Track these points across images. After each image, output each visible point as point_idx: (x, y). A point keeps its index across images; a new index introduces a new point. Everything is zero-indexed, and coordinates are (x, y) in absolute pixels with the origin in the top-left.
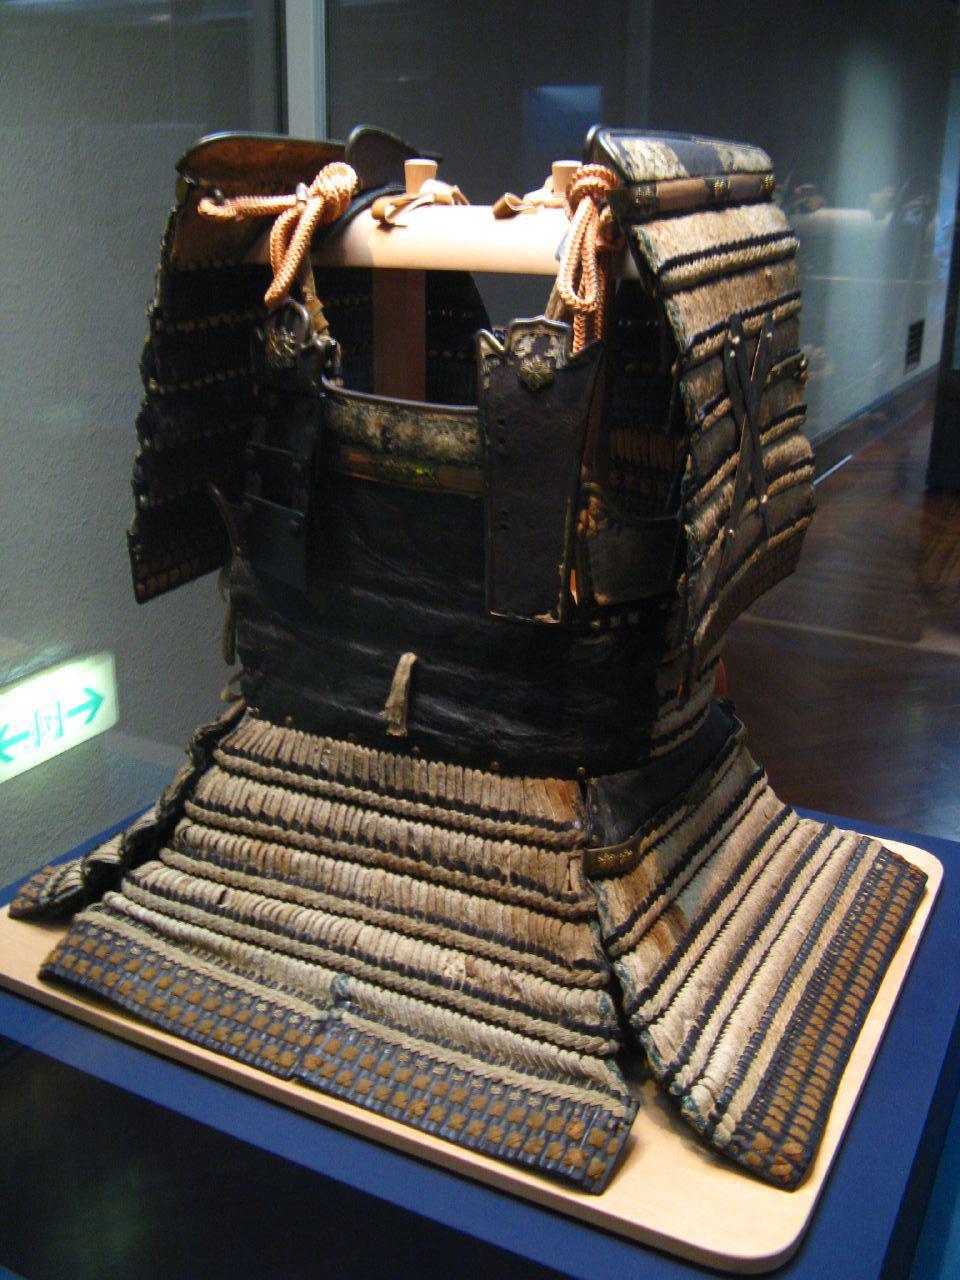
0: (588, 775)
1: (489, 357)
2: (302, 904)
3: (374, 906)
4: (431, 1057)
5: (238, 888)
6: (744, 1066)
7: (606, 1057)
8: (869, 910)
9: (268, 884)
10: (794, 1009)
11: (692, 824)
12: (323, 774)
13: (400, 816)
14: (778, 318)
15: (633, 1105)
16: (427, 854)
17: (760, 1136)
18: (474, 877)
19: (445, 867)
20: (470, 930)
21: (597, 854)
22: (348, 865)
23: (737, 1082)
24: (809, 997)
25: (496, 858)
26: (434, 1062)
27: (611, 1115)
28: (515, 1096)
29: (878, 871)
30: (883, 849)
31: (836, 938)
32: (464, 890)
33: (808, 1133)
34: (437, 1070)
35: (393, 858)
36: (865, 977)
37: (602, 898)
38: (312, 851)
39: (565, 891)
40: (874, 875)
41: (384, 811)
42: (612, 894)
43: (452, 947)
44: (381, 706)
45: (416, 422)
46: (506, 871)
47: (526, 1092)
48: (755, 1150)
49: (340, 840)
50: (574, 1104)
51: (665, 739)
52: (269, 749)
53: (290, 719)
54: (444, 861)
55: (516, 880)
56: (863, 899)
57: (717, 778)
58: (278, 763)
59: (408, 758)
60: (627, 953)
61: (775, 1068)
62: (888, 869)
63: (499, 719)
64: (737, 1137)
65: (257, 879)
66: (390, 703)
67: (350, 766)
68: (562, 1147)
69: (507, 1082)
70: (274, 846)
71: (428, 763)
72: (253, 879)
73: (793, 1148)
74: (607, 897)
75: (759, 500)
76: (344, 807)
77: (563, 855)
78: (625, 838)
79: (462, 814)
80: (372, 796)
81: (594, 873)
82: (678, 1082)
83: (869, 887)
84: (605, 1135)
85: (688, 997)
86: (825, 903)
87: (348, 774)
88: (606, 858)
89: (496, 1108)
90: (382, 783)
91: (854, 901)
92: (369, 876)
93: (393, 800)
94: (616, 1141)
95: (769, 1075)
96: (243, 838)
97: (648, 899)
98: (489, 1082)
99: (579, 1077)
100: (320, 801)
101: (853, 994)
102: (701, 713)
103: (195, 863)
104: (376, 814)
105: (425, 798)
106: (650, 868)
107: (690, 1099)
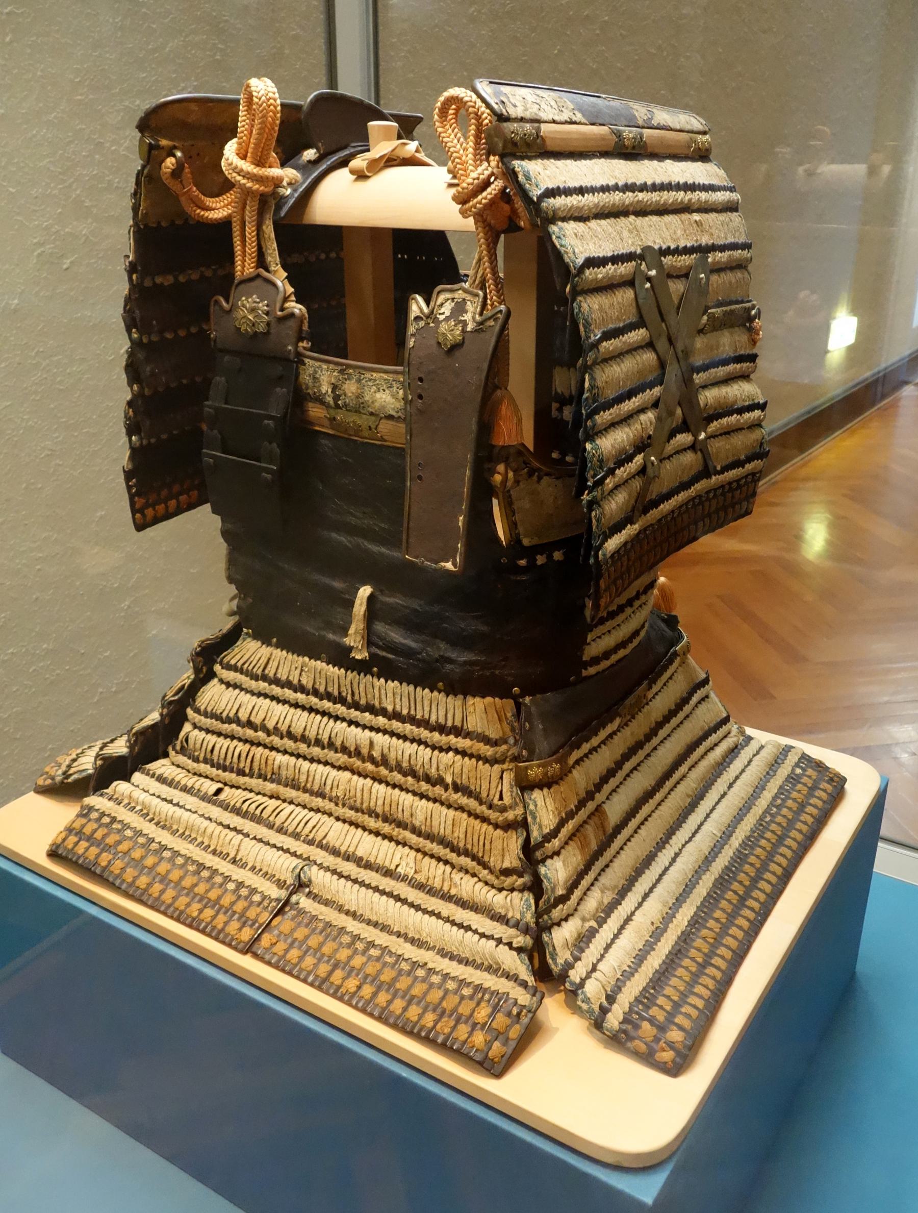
0: (523, 695)
1: (417, 318)
2: (284, 801)
3: (340, 805)
4: (369, 940)
5: (232, 786)
6: (640, 958)
7: (520, 950)
8: (785, 811)
9: (254, 782)
10: (699, 904)
11: (627, 731)
12: (300, 688)
13: (364, 727)
14: (714, 263)
15: (538, 995)
16: (384, 761)
17: (646, 1025)
18: (423, 783)
19: (399, 772)
20: (416, 831)
21: (527, 768)
22: (321, 767)
23: (628, 975)
24: (715, 893)
25: (441, 767)
26: (371, 944)
27: (516, 1003)
28: (436, 979)
29: (796, 775)
30: (804, 757)
31: (748, 838)
32: (415, 794)
33: (693, 1021)
34: (374, 952)
35: (357, 763)
36: (774, 873)
37: (532, 807)
38: (292, 754)
39: (496, 801)
40: (793, 779)
41: (351, 723)
42: (540, 802)
43: (405, 845)
44: (345, 631)
45: (359, 381)
46: (449, 780)
47: (446, 976)
48: (640, 1038)
49: (314, 745)
50: (486, 990)
51: (595, 661)
52: (258, 665)
53: (275, 640)
54: (399, 768)
55: (457, 788)
56: (779, 802)
57: (655, 689)
58: (264, 678)
59: (369, 677)
60: (551, 857)
61: (672, 960)
62: (807, 773)
63: (442, 645)
64: (624, 1027)
65: (247, 779)
66: (351, 631)
67: (324, 682)
68: (470, 1029)
69: (430, 965)
70: (260, 749)
71: (386, 682)
72: (242, 780)
73: (675, 1035)
74: (536, 806)
75: (696, 436)
76: (319, 717)
77: (497, 768)
78: (554, 753)
79: (414, 727)
80: (341, 709)
81: (525, 786)
82: (572, 977)
83: (787, 790)
84: (508, 1021)
85: (592, 903)
86: (741, 806)
87: (322, 689)
88: (535, 771)
89: (417, 990)
90: (349, 698)
91: (771, 803)
92: (337, 778)
93: (358, 713)
94: (517, 1027)
95: (664, 967)
96: (235, 742)
97: (576, 806)
98: (415, 965)
99: (494, 969)
100: (299, 711)
101: (760, 889)
102: (636, 633)
103: (195, 765)
104: (345, 724)
105: (383, 712)
106: (581, 778)
107: (582, 992)
